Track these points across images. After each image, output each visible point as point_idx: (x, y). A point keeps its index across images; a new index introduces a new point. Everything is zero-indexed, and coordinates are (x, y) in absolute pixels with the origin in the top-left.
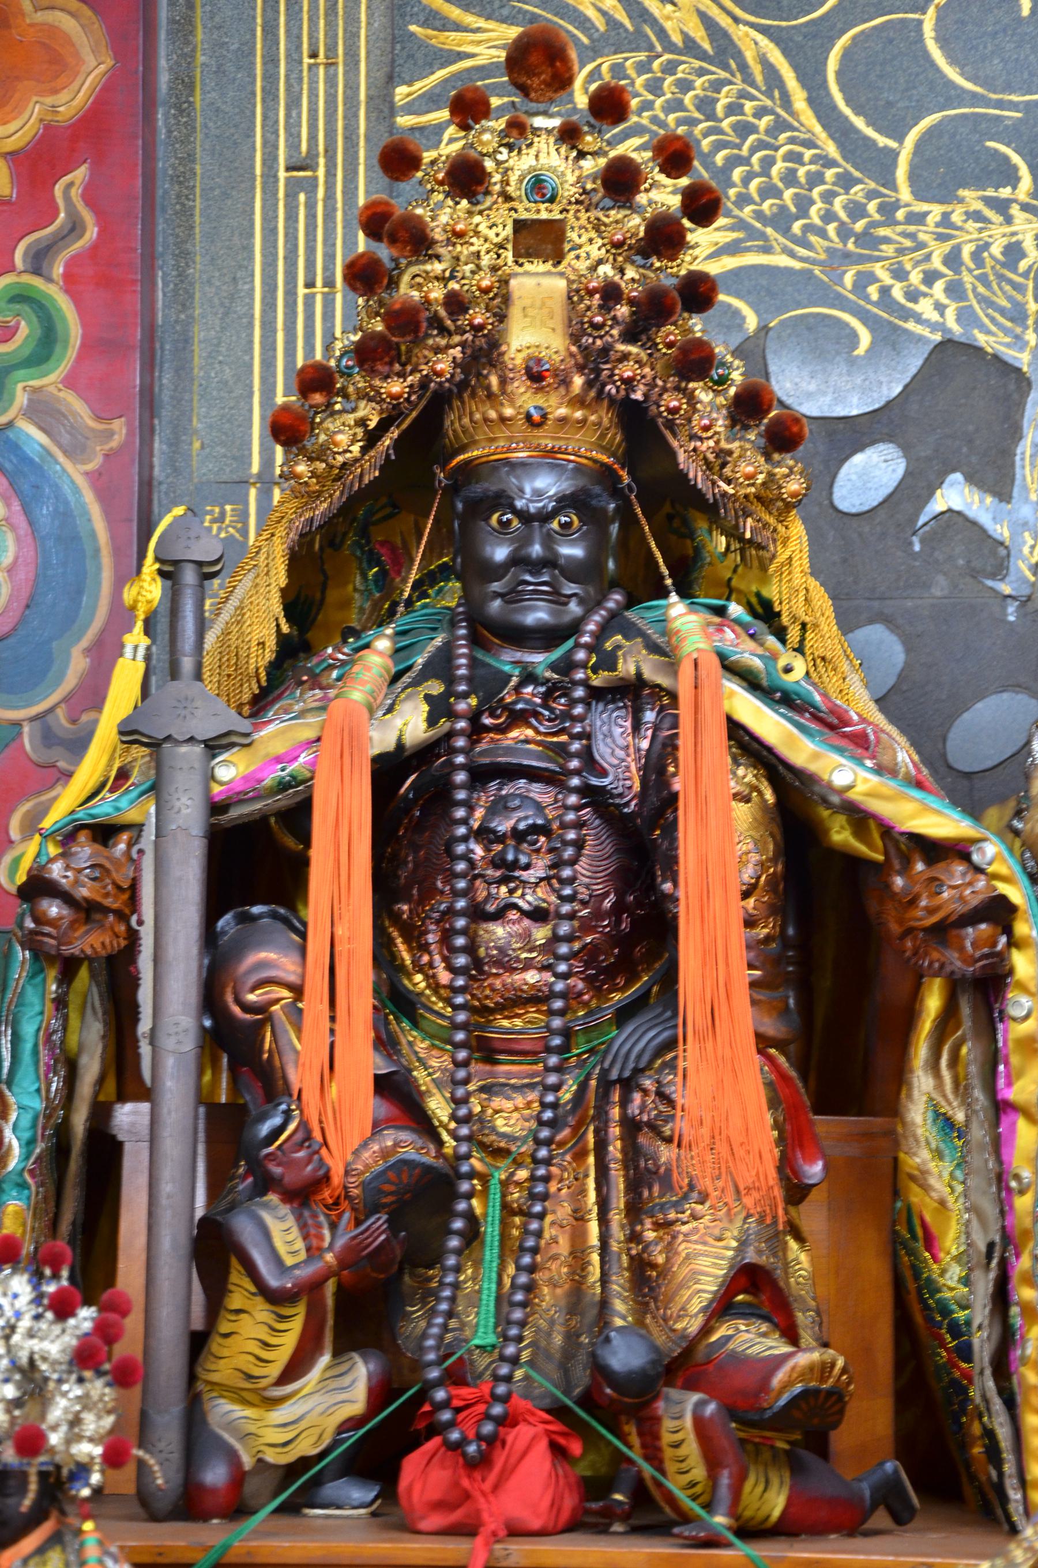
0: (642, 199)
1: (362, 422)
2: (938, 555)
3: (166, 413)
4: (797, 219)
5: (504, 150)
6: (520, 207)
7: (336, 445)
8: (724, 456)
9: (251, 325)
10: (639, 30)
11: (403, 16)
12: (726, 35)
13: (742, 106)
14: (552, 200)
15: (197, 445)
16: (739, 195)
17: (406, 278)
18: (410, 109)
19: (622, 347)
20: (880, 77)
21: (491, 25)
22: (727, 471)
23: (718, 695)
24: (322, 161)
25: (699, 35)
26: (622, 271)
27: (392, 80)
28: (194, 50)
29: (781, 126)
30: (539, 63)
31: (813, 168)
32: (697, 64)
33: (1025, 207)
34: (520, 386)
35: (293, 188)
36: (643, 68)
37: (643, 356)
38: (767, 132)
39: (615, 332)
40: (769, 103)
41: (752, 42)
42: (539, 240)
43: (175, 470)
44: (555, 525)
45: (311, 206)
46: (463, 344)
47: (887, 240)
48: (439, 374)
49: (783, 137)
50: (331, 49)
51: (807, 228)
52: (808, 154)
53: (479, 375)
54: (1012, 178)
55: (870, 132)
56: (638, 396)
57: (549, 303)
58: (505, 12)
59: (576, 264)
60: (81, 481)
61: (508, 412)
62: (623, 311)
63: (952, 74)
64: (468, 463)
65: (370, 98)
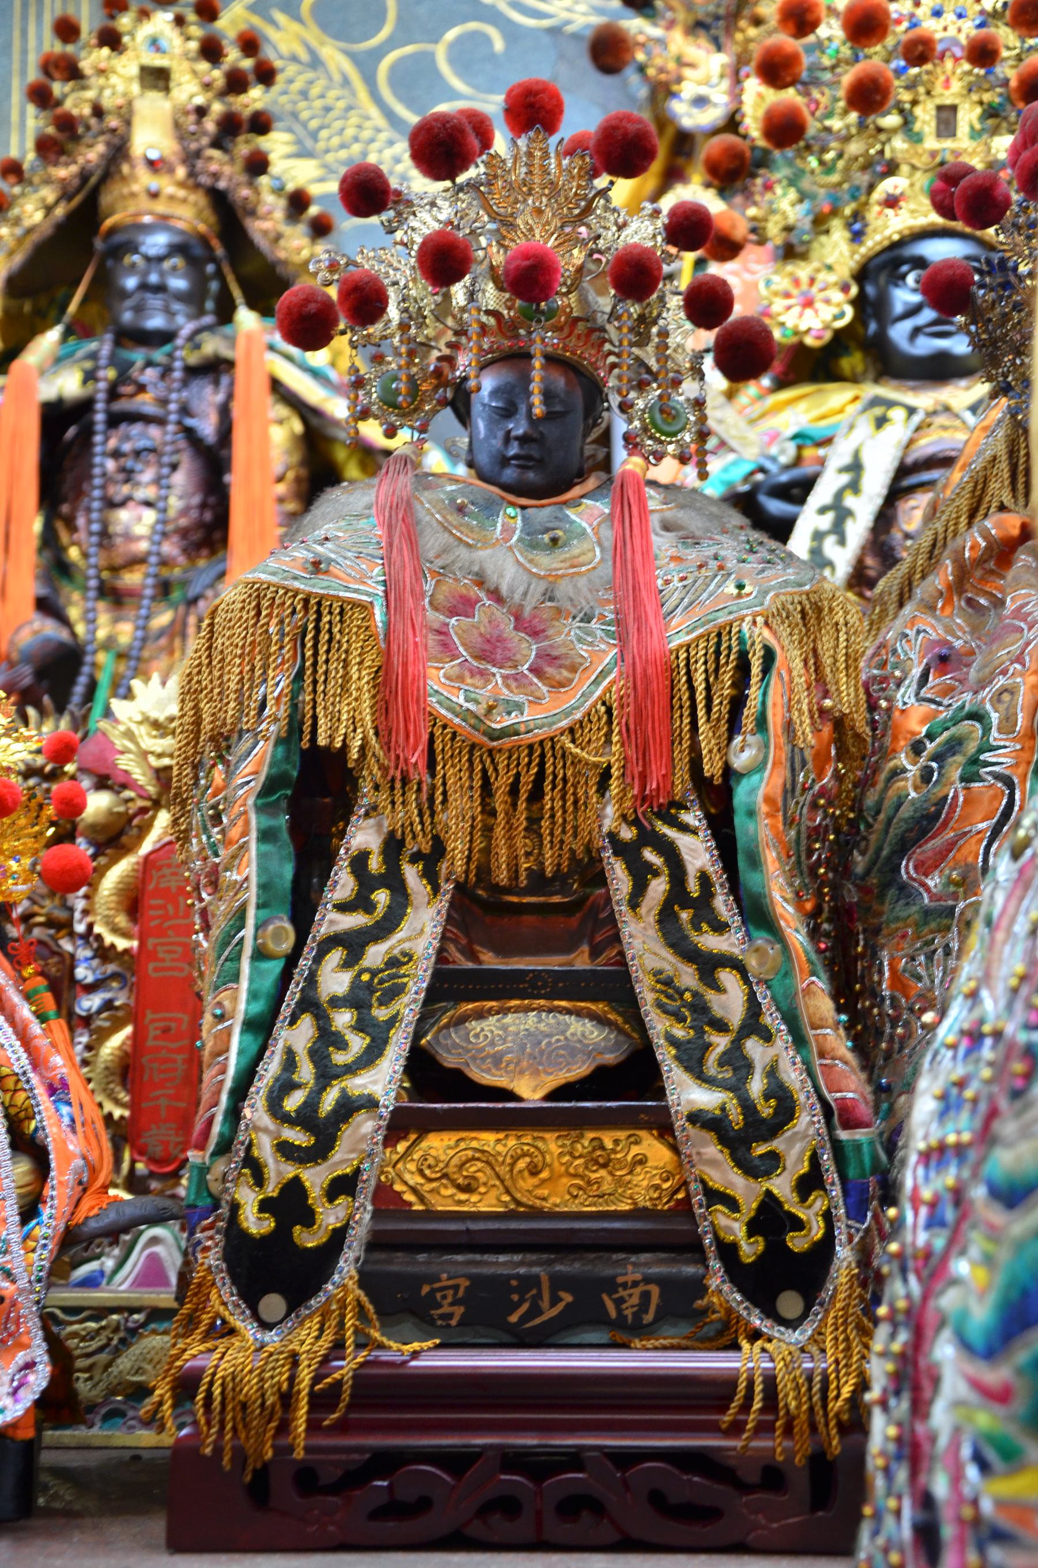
23: (262, 362)
42: (157, 78)
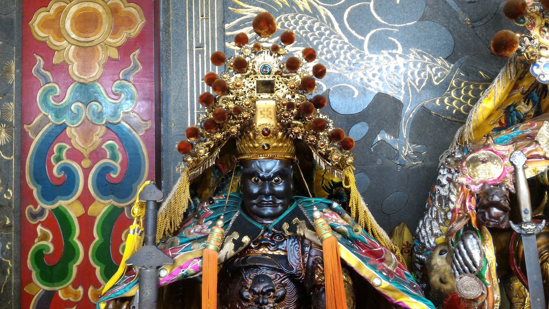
0: (300, 70)
1: (208, 146)
2: (378, 153)
3: (164, 116)
4: (337, 59)
5: (253, 54)
6: (259, 76)
7: (200, 153)
8: (328, 152)
9: (187, 91)
10: (291, 7)
11: (226, 5)
12: (316, 8)
13: (321, 28)
14: (269, 74)
15: (173, 125)
16: (320, 53)
17: (221, 100)
18: (229, 30)
19: (294, 122)
20: (359, 19)
21: (251, 7)
22: (329, 158)
24: (205, 45)
25: (308, 8)
26: (293, 97)
27: (224, 22)
28: (170, 16)
29: (331, 33)
30: (264, 24)
31: (341, 45)
32: (308, 16)
33: (400, 56)
34: (261, 137)
35: (198, 53)
36: (293, 18)
37: (302, 125)
38: (328, 35)
39: (292, 118)
40: (328, 27)
41: (323, 10)
43: (167, 132)
44: (273, 181)
45: (202, 58)
46: (241, 123)
47: (362, 65)
48: (233, 133)
49: (332, 37)
50: (207, 14)
51: (340, 62)
52: (339, 41)
53: (246, 132)
54: (396, 47)
55: (356, 35)
56: (300, 137)
57: (269, 110)
58: (255, 3)
59: (279, 94)
60: (139, 138)
61: (257, 145)
62: (295, 111)
63: (379, 18)
64: (244, 159)
65: (218, 28)
